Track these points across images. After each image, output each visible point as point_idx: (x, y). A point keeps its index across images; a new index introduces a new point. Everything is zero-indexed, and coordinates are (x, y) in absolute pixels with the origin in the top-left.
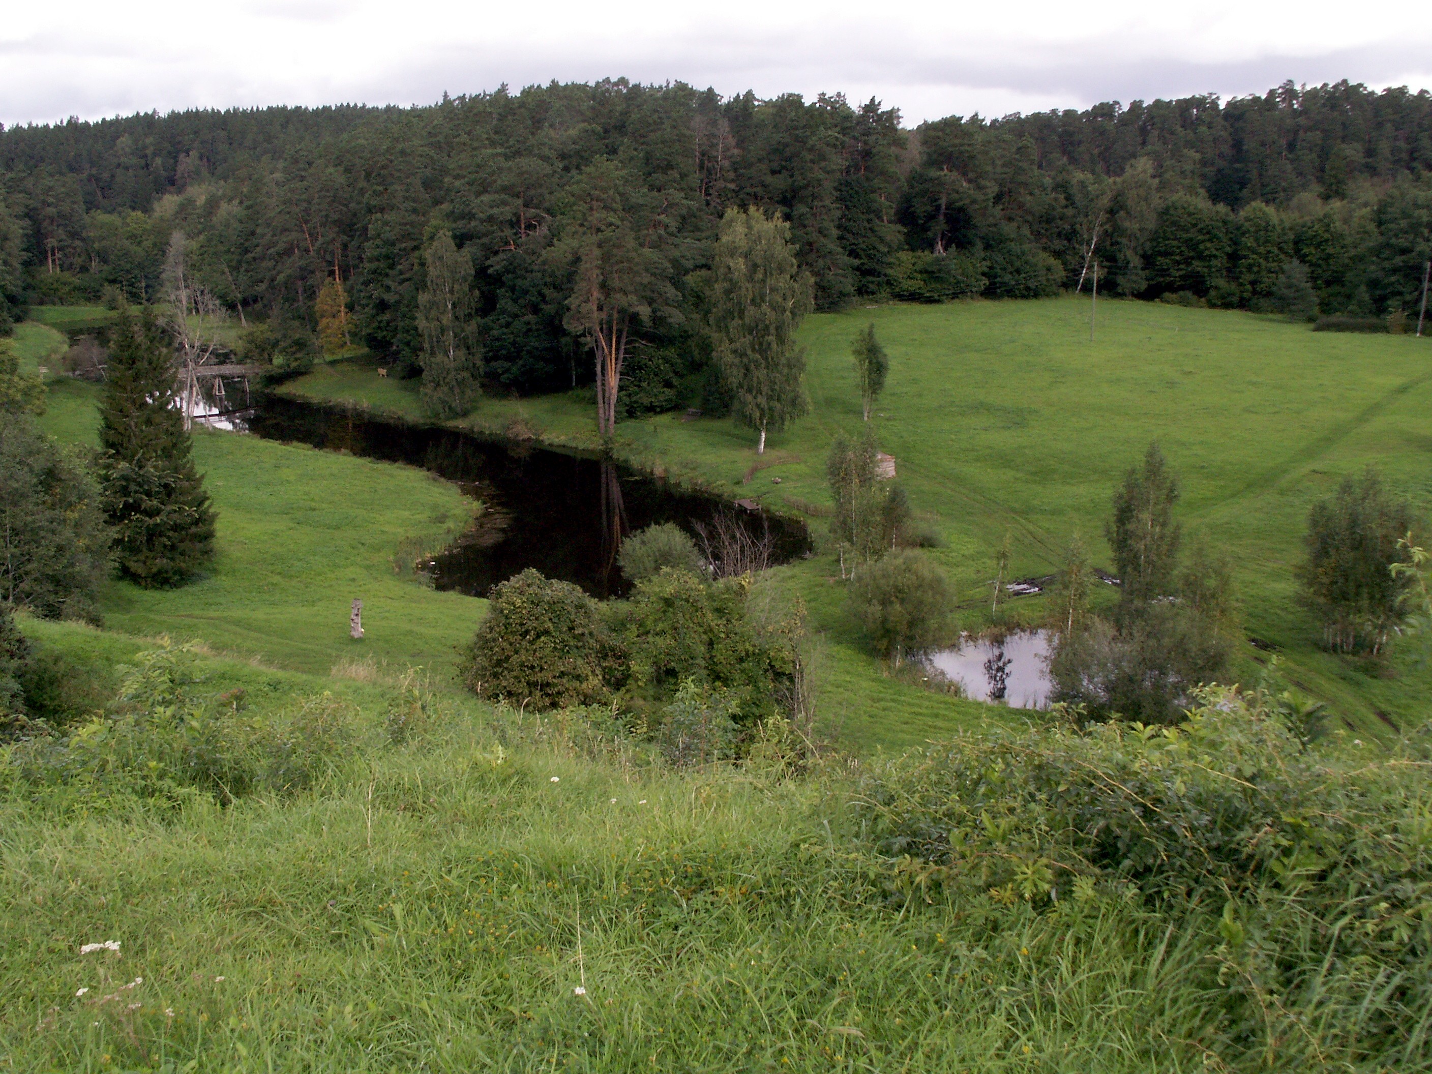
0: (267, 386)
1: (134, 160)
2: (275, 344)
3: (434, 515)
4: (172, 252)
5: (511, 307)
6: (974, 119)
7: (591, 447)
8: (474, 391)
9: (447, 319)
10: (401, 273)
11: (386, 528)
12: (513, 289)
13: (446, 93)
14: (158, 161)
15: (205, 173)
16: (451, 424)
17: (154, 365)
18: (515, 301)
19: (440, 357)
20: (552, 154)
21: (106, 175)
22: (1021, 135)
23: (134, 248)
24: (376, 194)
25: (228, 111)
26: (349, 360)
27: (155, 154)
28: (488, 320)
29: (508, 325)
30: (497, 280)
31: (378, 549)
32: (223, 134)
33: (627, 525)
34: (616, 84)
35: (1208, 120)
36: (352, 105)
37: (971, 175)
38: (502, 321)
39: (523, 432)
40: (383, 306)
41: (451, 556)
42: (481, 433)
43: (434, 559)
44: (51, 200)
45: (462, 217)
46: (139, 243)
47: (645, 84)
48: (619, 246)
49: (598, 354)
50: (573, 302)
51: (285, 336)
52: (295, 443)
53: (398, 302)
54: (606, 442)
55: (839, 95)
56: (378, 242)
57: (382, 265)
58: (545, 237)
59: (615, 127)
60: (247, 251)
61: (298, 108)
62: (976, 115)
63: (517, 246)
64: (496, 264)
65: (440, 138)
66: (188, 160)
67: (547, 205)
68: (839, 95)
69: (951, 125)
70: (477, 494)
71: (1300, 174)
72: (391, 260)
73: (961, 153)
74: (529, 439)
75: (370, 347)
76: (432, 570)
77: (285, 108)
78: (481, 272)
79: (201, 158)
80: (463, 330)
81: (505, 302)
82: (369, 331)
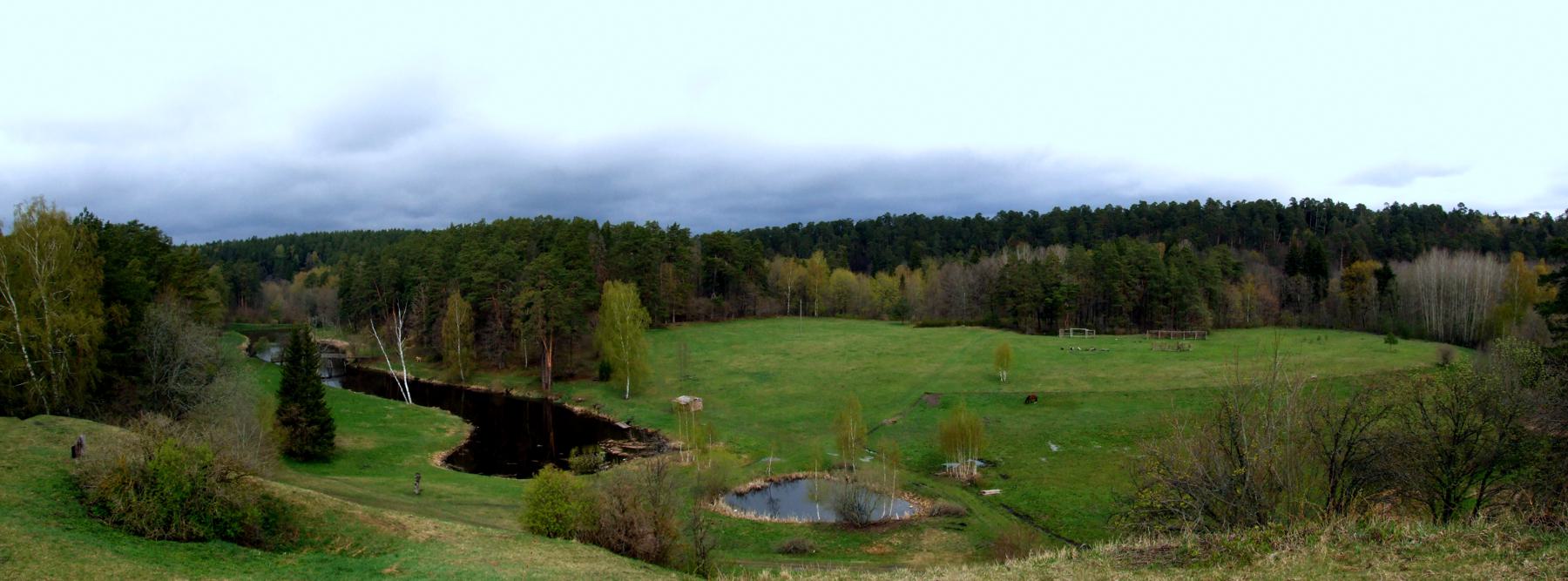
15: (320, 261)
27: (295, 253)
34: (545, 218)
48: (553, 297)
67: (511, 276)
69: (718, 236)
73: (724, 249)
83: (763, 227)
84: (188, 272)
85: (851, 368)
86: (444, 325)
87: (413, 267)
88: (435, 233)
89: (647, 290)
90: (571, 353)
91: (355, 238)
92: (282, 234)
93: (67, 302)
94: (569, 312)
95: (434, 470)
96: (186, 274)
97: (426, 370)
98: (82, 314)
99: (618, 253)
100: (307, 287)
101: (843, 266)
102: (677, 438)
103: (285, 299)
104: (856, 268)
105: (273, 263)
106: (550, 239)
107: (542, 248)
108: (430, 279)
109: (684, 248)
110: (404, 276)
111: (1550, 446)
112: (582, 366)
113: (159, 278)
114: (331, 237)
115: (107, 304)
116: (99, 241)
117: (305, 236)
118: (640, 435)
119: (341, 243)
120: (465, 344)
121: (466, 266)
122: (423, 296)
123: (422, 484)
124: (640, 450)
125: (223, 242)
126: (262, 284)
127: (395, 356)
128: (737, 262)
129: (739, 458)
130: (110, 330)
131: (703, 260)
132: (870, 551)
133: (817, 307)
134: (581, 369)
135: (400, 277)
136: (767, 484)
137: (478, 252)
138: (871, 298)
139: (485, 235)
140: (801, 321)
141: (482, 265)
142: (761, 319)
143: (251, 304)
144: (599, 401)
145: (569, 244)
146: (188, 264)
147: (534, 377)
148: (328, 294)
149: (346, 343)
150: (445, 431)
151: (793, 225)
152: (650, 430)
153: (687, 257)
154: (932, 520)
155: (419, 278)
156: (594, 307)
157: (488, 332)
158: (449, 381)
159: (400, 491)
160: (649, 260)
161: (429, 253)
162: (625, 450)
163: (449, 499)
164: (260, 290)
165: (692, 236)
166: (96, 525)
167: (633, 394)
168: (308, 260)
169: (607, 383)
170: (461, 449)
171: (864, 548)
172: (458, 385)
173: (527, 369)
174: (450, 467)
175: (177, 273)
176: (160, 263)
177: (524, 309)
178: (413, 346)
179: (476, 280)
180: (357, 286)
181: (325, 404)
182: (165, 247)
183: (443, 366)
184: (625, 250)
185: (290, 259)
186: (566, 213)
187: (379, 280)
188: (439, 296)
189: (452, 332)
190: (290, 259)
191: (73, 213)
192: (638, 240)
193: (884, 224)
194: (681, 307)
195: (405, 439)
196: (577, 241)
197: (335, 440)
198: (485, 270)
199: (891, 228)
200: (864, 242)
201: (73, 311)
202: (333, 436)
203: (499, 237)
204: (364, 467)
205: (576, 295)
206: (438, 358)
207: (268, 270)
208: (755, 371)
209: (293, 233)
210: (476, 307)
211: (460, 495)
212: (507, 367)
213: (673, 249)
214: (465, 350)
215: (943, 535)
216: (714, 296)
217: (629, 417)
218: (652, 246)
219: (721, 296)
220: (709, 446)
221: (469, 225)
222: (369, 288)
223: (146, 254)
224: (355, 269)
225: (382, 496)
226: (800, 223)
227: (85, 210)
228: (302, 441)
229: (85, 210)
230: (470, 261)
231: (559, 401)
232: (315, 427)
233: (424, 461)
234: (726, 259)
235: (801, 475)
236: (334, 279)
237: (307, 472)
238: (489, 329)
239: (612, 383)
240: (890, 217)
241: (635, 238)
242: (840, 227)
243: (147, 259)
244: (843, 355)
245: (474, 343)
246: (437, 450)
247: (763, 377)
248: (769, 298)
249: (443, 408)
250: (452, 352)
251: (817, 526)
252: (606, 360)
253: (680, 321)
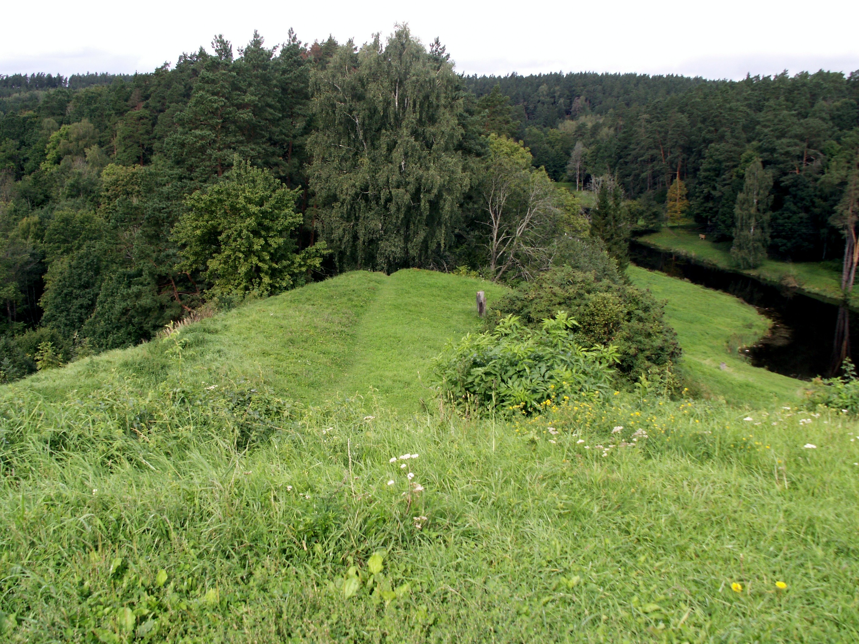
0: (633, 237)
1: (548, 99)
2: (641, 213)
3: (745, 323)
4: (573, 154)
5: (793, 208)
7: (835, 297)
8: (762, 254)
9: (753, 211)
10: (724, 180)
11: (719, 327)
12: (795, 196)
13: (256, 32)
14: (562, 100)
15: (588, 109)
16: (746, 272)
18: (795, 204)
19: (745, 233)
20: (827, 117)
21: (531, 106)
23: (550, 149)
24: (709, 132)
26: (682, 227)
27: (560, 97)
28: (777, 213)
29: (789, 218)
30: (786, 190)
31: (716, 337)
32: (600, 87)
38: (786, 215)
39: (792, 283)
40: (708, 198)
41: (758, 348)
42: (765, 280)
43: (748, 348)
45: (766, 150)
46: (553, 147)
49: (848, 242)
50: (839, 208)
51: (647, 209)
52: (657, 271)
53: (721, 197)
54: (845, 295)
56: (710, 160)
57: (712, 174)
58: (819, 167)
60: (620, 158)
63: (800, 171)
64: (786, 180)
65: (752, 102)
66: (579, 101)
67: (822, 147)
70: (768, 315)
72: (718, 172)
74: (795, 287)
75: (696, 221)
76: (747, 354)
78: (777, 183)
79: (586, 100)
80: (761, 218)
81: (789, 204)
82: (698, 211)
91: (629, 83)
111: (541, 364)
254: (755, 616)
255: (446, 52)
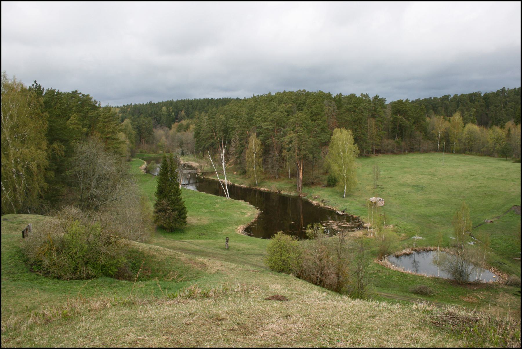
6: (407, 100)
15: (186, 116)
17: (172, 170)
22: (421, 105)
25: (193, 100)
27: (172, 112)
33: (249, 234)
34: (302, 92)
35: (477, 99)
36: (227, 98)
37: (406, 117)
44: (144, 124)
47: (310, 91)
55: (367, 94)
59: (302, 103)
61: (212, 99)
62: (407, 99)
68: (367, 94)
69: (400, 102)
71: (507, 115)
77: (208, 98)
83: (428, 97)
84: (107, 122)
85: (470, 186)
86: (247, 153)
87: (232, 120)
88: (245, 100)
89: (360, 134)
90: (313, 170)
92: (165, 100)
93: (23, 142)
94: (311, 146)
95: (237, 236)
96: (105, 124)
97: (238, 179)
98: (33, 149)
99: (345, 112)
100: (178, 131)
101: (473, 122)
102: (368, 222)
103: (166, 138)
104: (480, 124)
105: (161, 117)
106: (304, 103)
107: (300, 109)
108: (241, 126)
109: (381, 110)
110: (227, 125)
112: (318, 177)
113: (90, 126)
114: (192, 103)
115: (51, 142)
116: (45, 103)
117: (178, 101)
118: (348, 218)
119: (197, 106)
120: (258, 164)
121: (258, 119)
122: (237, 137)
123: (230, 243)
124: (349, 227)
125: (133, 105)
126: (154, 130)
127: (221, 172)
128: (410, 119)
129: (400, 235)
130: (53, 158)
131: (391, 117)
132: (464, 299)
133: (455, 147)
134: (318, 179)
135: (226, 126)
136: (413, 252)
137: (265, 111)
138: (488, 142)
139: (270, 101)
140: (444, 156)
141: (267, 119)
142: (423, 153)
143: (148, 142)
144: (326, 199)
145: (313, 106)
146: (106, 118)
147: (293, 184)
148: (189, 135)
149: (198, 164)
150: (245, 214)
151: (445, 96)
152: (354, 216)
153: (383, 115)
154: (506, 287)
155: (235, 126)
156: (326, 143)
157: (270, 158)
158: (250, 185)
159: (218, 248)
160: (362, 117)
161: (240, 111)
162: (340, 227)
163: (243, 252)
164: (153, 133)
165: (387, 103)
166: (34, 276)
167: (348, 195)
168: (179, 115)
169: (333, 188)
170: (253, 224)
171: (461, 297)
172: (254, 188)
173: (290, 179)
174: (246, 234)
175: (100, 123)
176: (91, 118)
177: (289, 144)
178: (232, 166)
179: (264, 127)
180: (204, 131)
181: (181, 199)
182: (94, 108)
183: (247, 177)
184: (349, 110)
185: (170, 115)
186: (312, 88)
187: (215, 127)
188: (245, 136)
189: (251, 157)
190: (170, 115)
191: (28, 85)
192: (356, 105)
193: (501, 95)
194: (378, 145)
195: (224, 218)
196: (317, 105)
197: (187, 219)
198: (268, 121)
199: (505, 97)
200: (487, 107)
201: (27, 148)
202: (185, 217)
203: (277, 102)
204: (202, 234)
205: (314, 137)
206: (244, 173)
207: (158, 121)
208: (415, 185)
209: (171, 100)
210: (263, 143)
211: (249, 249)
212: (279, 178)
213: (375, 110)
214: (258, 167)
215: (511, 299)
216: (397, 139)
217: (344, 208)
218: (364, 108)
219: (400, 139)
220: (384, 228)
221: (263, 95)
222: (209, 132)
223: (80, 112)
224: (203, 121)
225: (209, 250)
226: (449, 95)
227: (35, 82)
228: (170, 220)
229: (35, 82)
230: (261, 116)
231: (306, 198)
232: (176, 212)
233: (233, 230)
234: (404, 116)
235: (432, 248)
236: (193, 127)
237: (172, 238)
238: (271, 156)
239: (337, 188)
240: (505, 90)
241: (355, 104)
242: (473, 98)
243: (82, 114)
244: (467, 178)
245: (263, 163)
246: (240, 224)
247: (419, 188)
248: (428, 140)
249: (245, 201)
250: (251, 169)
251: (436, 280)
252: (333, 175)
253: (378, 153)
254: (115, 262)
255: (42, 87)
